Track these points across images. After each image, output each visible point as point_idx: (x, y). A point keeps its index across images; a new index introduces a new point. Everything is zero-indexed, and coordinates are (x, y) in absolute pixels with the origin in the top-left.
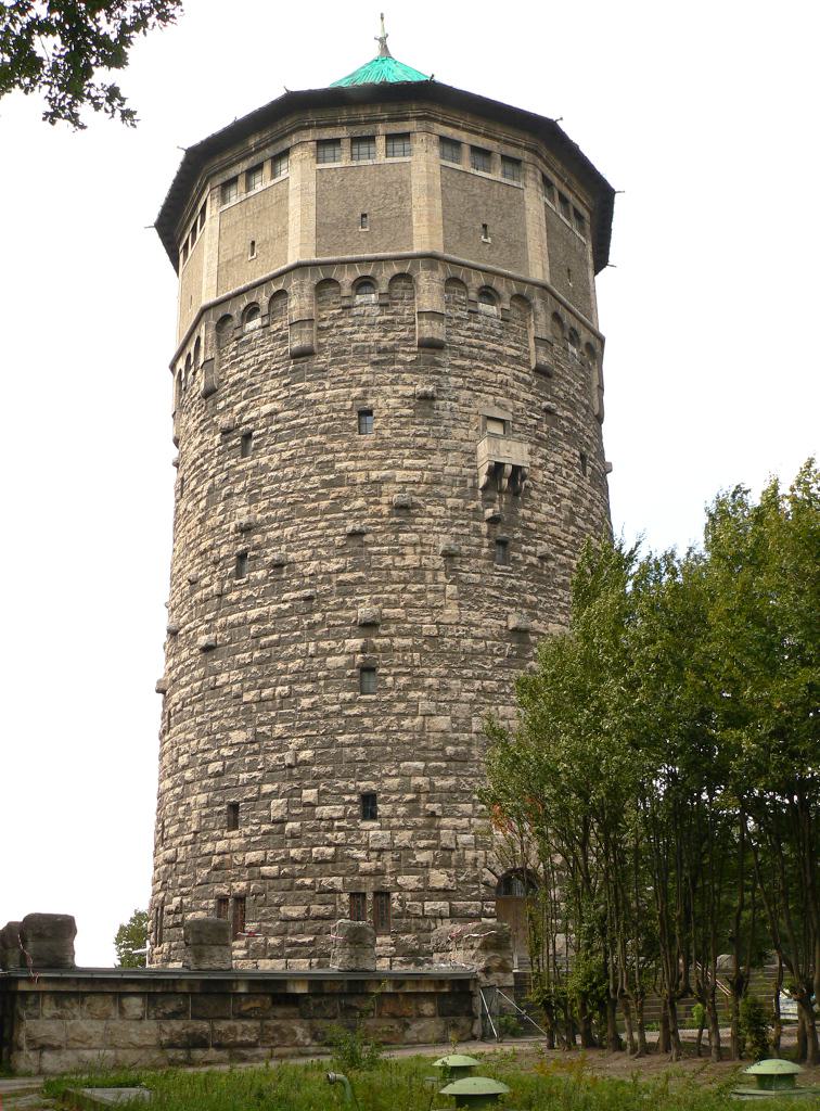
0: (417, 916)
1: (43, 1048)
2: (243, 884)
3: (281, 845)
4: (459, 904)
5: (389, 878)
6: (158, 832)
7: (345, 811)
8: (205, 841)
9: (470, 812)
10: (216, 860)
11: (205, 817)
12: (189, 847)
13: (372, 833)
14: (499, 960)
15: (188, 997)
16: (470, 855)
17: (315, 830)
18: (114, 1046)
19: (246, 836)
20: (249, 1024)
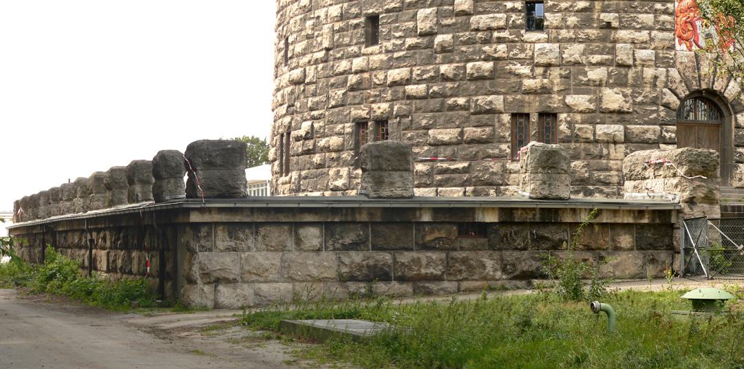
0: (587, 141)
1: (218, 281)
2: (385, 106)
3: (430, 60)
4: (635, 128)
5: (556, 97)
6: (279, 50)
7: (507, 20)
8: (339, 58)
9: (650, 24)
10: (353, 79)
11: (338, 31)
12: (321, 66)
13: (538, 46)
14: (705, 190)
15: (367, 227)
16: (649, 73)
17: (469, 42)
18: (291, 279)
19: (387, 51)
20: (434, 256)
